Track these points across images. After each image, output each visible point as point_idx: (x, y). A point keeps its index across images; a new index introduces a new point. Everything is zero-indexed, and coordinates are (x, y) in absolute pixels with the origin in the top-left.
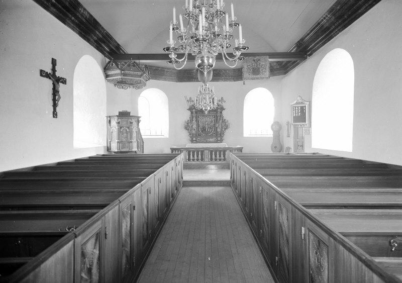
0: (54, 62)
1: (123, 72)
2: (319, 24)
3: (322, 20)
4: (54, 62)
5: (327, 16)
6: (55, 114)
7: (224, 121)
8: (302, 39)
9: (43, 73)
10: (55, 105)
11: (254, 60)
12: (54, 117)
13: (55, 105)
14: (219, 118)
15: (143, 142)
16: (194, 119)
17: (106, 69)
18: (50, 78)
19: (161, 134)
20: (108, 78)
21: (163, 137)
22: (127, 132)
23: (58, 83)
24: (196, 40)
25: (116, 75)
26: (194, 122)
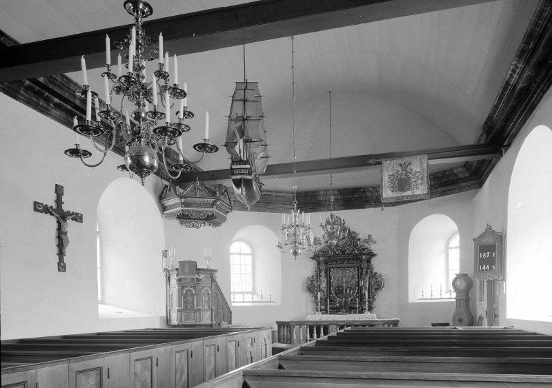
0: (59, 191)
1: (183, 200)
2: (507, 83)
3: (511, 76)
4: (59, 191)
5: (517, 67)
6: (62, 267)
7: (374, 275)
8: (490, 118)
9: (39, 208)
10: (61, 254)
11: (401, 165)
12: (59, 270)
13: (61, 254)
14: (365, 270)
15: (231, 313)
16: (323, 273)
17: (161, 197)
18: (52, 214)
19: (251, 300)
20: (166, 212)
21: (273, 304)
22: (192, 295)
23: (65, 220)
24: (294, 143)
25: (175, 206)
26: (323, 278)
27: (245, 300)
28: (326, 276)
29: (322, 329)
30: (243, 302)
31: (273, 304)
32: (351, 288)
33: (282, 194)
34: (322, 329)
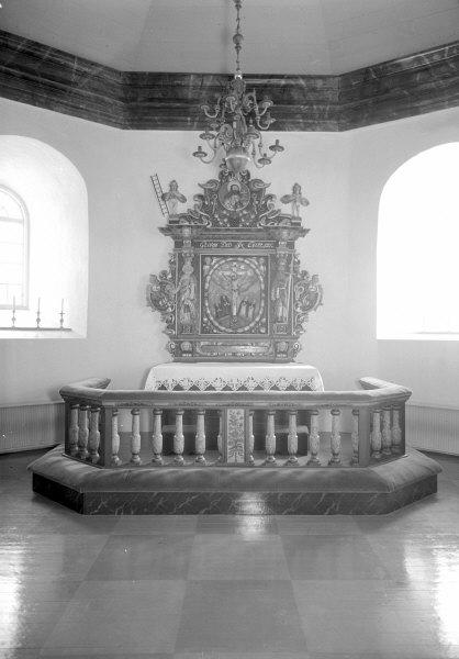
7: (302, 279)
16: (188, 267)
21: (64, 335)
27: (42, 325)
28: (195, 273)
29: (201, 421)
30: (38, 329)
31: (64, 335)
32: (248, 304)
33: (283, 82)
34: (201, 421)
